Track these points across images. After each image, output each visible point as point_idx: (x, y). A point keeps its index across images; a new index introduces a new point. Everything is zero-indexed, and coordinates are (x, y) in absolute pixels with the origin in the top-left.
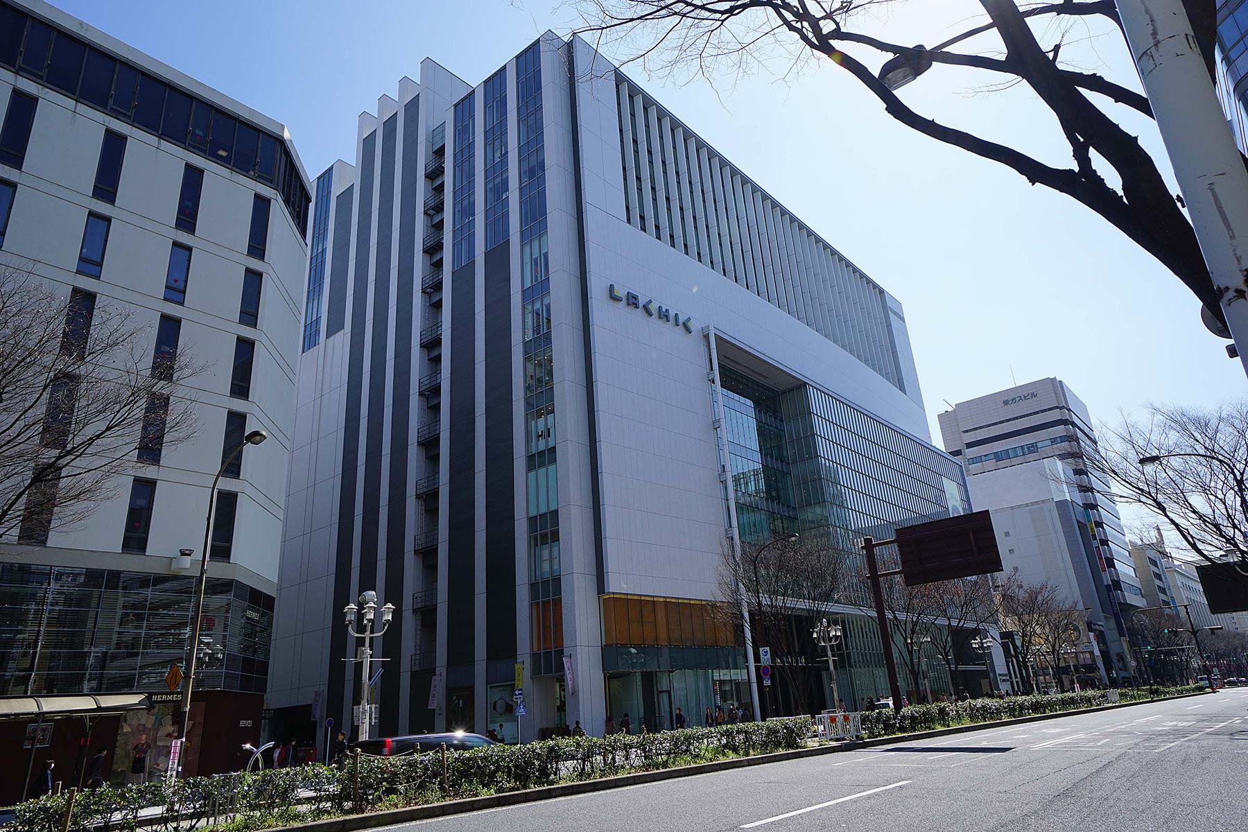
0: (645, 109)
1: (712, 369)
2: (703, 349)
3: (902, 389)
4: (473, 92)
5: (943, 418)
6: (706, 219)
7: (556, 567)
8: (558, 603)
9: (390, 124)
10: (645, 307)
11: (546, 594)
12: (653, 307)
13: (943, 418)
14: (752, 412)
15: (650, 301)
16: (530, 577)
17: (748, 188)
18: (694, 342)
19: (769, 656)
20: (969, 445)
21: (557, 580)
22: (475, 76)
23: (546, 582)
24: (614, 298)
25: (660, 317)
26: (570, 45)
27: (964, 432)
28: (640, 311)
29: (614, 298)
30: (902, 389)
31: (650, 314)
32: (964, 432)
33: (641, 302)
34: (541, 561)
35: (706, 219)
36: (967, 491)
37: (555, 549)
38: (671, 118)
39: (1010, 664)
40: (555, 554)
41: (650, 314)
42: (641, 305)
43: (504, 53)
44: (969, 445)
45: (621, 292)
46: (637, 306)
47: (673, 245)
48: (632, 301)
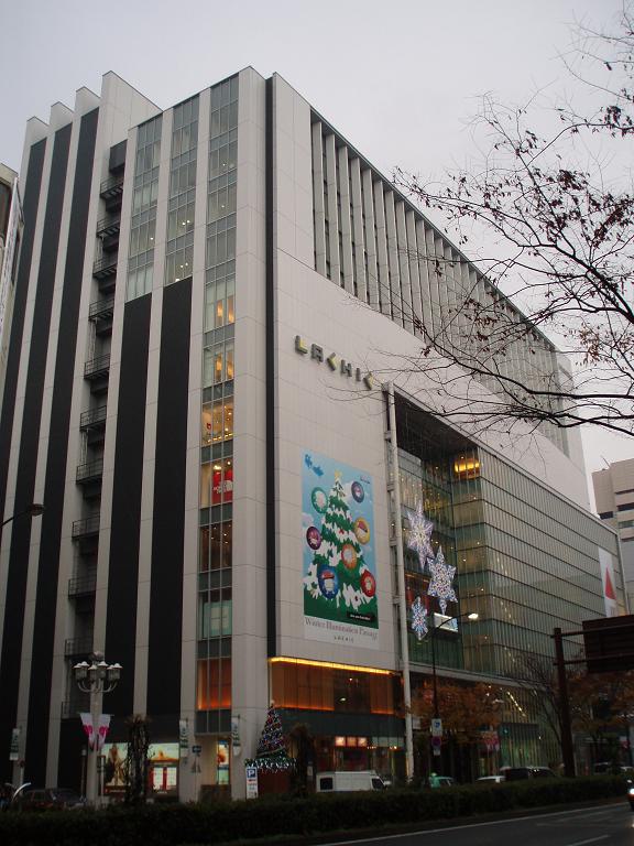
0: (324, 137)
1: (389, 428)
2: (381, 406)
3: (566, 452)
4: (161, 115)
5: (594, 475)
6: (327, 214)
7: (226, 626)
8: (228, 663)
9: (63, 135)
10: (329, 361)
11: (214, 652)
12: (336, 362)
13: (594, 475)
14: (419, 472)
15: (333, 355)
16: (197, 636)
17: (357, 162)
18: (375, 404)
19: (440, 727)
20: (622, 508)
21: (228, 640)
22: (166, 98)
23: (214, 641)
24: (300, 351)
25: (342, 372)
26: (269, 84)
27: (618, 493)
28: (324, 365)
29: (300, 351)
30: (566, 452)
31: (332, 368)
32: (618, 493)
33: (326, 355)
34: (210, 619)
35: (327, 214)
36: (620, 562)
37: (226, 609)
38: (361, 159)
39: (39, 498)
40: (226, 612)
41: (332, 368)
42: (325, 359)
43: (199, 79)
44: (622, 508)
45: (306, 344)
46: (320, 359)
47: (329, 276)
48: (317, 354)
